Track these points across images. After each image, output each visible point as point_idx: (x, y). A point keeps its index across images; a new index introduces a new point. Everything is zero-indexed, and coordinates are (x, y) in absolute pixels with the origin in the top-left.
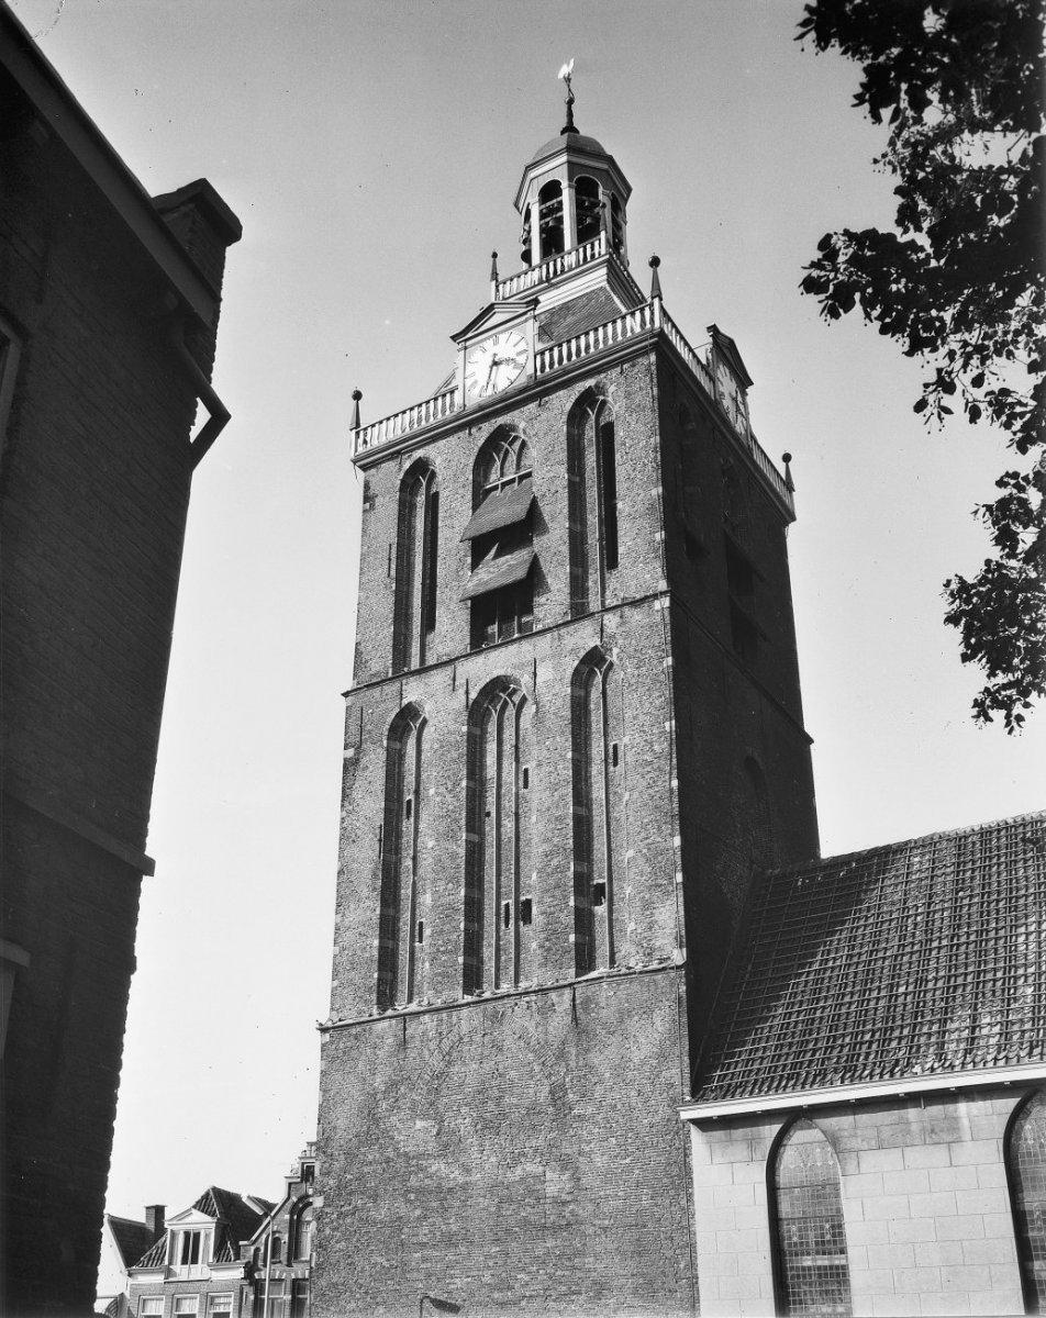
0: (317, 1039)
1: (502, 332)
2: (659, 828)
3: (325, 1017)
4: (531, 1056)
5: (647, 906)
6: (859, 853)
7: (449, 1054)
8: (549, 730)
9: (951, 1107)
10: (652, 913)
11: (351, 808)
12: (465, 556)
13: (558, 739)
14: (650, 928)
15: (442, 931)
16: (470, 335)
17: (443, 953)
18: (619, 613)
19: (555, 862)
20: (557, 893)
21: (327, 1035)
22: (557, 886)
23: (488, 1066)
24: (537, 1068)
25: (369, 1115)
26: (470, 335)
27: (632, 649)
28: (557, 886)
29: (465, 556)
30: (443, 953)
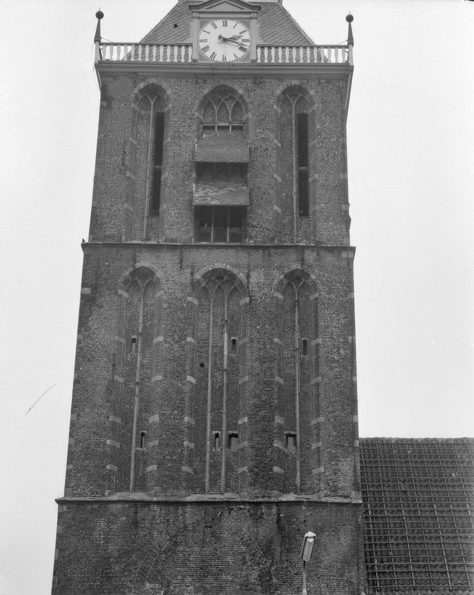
0: (56, 506)
1: (230, 19)
2: (343, 408)
3: (61, 495)
4: (243, 548)
5: (334, 457)
6: (417, 440)
7: (175, 536)
8: (259, 317)
9: (118, 499)
10: (336, 464)
11: (87, 333)
12: (191, 171)
13: (267, 326)
14: (335, 474)
15: (168, 445)
16: (203, 10)
17: (169, 460)
18: (178, 253)
19: (262, 413)
20: (265, 435)
21: (65, 507)
22: (264, 431)
23: (208, 550)
24: (248, 557)
25: (102, 573)
26: (203, 10)
27: (324, 279)
28: (264, 431)
29: (191, 171)
30: (169, 460)
